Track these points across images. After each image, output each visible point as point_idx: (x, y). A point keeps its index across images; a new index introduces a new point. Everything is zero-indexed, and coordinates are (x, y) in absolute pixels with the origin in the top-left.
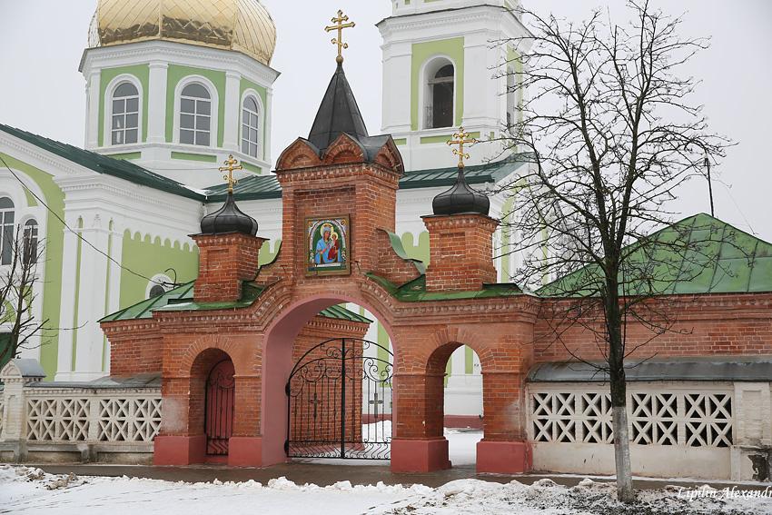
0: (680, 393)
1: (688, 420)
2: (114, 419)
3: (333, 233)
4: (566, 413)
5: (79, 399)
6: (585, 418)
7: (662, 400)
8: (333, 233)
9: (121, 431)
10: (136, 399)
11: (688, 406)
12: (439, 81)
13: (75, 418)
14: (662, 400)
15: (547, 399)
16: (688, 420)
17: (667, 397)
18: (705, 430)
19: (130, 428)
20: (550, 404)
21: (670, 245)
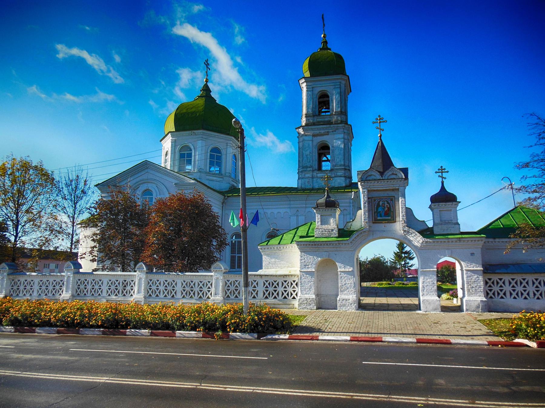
0: (507, 278)
1: (283, 289)
2: (82, 287)
3: (386, 204)
4: (501, 286)
5: (171, 280)
6: (505, 288)
7: (499, 281)
8: (386, 204)
9: (157, 293)
10: (39, 280)
11: (510, 283)
12: (321, 100)
13: (97, 287)
14: (499, 281)
15: (492, 281)
16: (160, 288)
17: (501, 279)
18: (494, 292)
19: (50, 291)
20: (153, 283)
21: (75, 204)
